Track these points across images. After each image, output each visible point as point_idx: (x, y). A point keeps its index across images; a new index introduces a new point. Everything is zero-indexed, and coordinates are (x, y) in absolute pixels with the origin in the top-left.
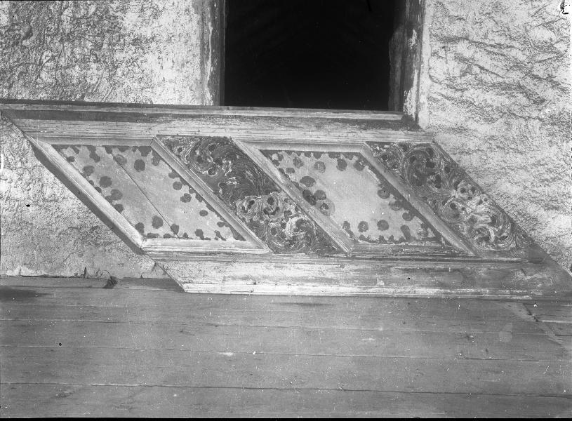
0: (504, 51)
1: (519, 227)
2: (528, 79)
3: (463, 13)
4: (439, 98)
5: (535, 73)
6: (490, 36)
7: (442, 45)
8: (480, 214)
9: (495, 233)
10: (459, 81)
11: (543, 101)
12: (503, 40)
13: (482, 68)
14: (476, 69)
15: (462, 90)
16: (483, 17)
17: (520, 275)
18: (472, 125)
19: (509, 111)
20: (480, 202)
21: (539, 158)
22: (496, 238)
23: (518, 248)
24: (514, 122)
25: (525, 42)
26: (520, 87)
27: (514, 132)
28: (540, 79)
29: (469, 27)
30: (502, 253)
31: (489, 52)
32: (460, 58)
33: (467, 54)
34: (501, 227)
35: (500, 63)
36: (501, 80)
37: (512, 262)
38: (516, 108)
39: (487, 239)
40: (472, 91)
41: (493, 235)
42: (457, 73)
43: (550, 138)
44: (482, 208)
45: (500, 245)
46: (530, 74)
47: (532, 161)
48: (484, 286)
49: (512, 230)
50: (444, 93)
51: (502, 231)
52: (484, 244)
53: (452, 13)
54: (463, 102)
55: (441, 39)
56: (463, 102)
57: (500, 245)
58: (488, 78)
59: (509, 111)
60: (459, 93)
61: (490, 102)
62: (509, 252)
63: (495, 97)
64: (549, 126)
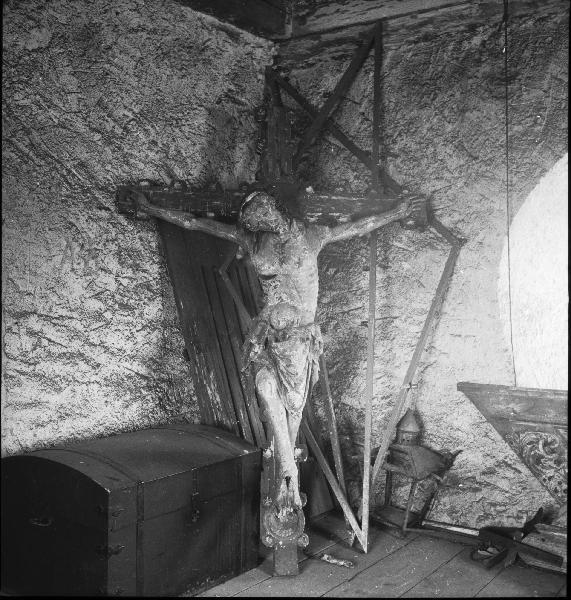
0: (66, 322)
1: (516, 452)
2: (87, 347)
3: (31, 289)
4: (14, 374)
5: (91, 341)
6: (54, 309)
7: (15, 321)
8: (551, 467)
9: (537, 448)
10: (31, 355)
11: (98, 365)
12: (64, 312)
13: (50, 340)
14: (45, 342)
15: (35, 364)
16: (48, 292)
17: (517, 408)
18: (44, 397)
19: (74, 378)
20: (550, 478)
21: (99, 418)
22: (537, 443)
23: (518, 433)
24: (78, 389)
25: (82, 313)
26: (82, 355)
27: (78, 400)
28: (95, 345)
29: (36, 302)
30: (532, 429)
31: (55, 325)
32: (31, 333)
33: (37, 327)
34: (532, 453)
35: (64, 335)
36: (65, 350)
37: (525, 421)
38: (79, 374)
39: (546, 444)
40: (42, 363)
41: (540, 446)
42: (29, 347)
43: (105, 399)
44: (550, 473)
45: (534, 436)
46: (87, 341)
47: (94, 422)
48: (551, 401)
49: (522, 449)
50: (19, 368)
51: (531, 450)
52: (549, 440)
53: (21, 289)
54: (36, 375)
55: (14, 315)
56: (36, 375)
57: (534, 436)
58: (55, 350)
59: (74, 378)
60: (32, 367)
61: (57, 372)
62: (527, 430)
63: (61, 368)
64: (104, 388)
